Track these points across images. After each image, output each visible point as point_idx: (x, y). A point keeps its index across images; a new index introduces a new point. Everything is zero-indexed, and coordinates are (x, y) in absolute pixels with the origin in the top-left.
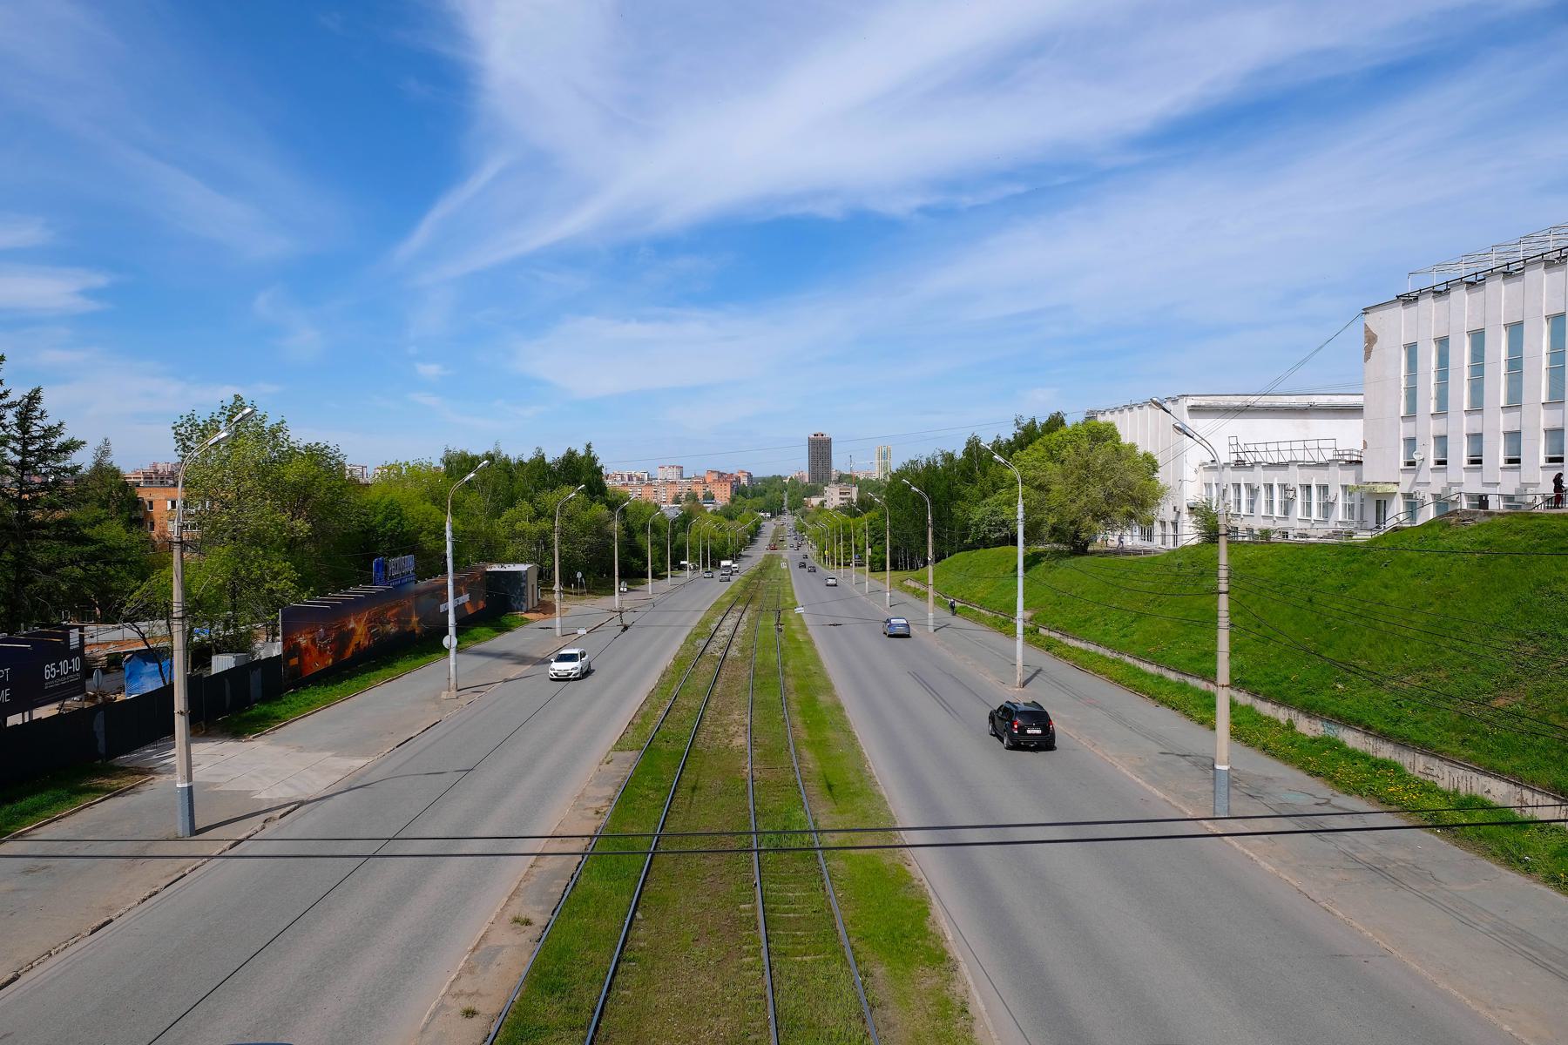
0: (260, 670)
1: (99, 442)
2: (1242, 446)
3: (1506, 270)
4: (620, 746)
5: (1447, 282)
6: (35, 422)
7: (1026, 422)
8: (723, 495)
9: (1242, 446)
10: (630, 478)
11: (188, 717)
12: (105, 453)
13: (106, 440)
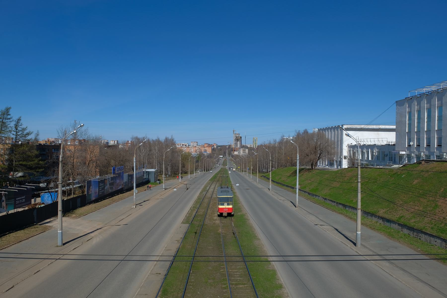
0: (80, 198)
1: (35, 132)
2: (360, 140)
3: (437, 91)
4: (183, 223)
5: (420, 94)
6: (19, 126)
7: (298, 131)
8: (209, 150)
9: (360, 140)
10: (183, 145)
11: (62, 211)
12: (38, 135)
13: (38, 131)
